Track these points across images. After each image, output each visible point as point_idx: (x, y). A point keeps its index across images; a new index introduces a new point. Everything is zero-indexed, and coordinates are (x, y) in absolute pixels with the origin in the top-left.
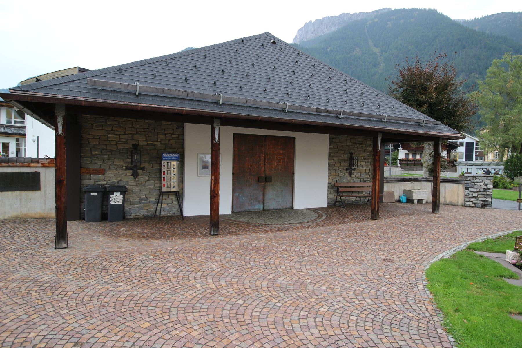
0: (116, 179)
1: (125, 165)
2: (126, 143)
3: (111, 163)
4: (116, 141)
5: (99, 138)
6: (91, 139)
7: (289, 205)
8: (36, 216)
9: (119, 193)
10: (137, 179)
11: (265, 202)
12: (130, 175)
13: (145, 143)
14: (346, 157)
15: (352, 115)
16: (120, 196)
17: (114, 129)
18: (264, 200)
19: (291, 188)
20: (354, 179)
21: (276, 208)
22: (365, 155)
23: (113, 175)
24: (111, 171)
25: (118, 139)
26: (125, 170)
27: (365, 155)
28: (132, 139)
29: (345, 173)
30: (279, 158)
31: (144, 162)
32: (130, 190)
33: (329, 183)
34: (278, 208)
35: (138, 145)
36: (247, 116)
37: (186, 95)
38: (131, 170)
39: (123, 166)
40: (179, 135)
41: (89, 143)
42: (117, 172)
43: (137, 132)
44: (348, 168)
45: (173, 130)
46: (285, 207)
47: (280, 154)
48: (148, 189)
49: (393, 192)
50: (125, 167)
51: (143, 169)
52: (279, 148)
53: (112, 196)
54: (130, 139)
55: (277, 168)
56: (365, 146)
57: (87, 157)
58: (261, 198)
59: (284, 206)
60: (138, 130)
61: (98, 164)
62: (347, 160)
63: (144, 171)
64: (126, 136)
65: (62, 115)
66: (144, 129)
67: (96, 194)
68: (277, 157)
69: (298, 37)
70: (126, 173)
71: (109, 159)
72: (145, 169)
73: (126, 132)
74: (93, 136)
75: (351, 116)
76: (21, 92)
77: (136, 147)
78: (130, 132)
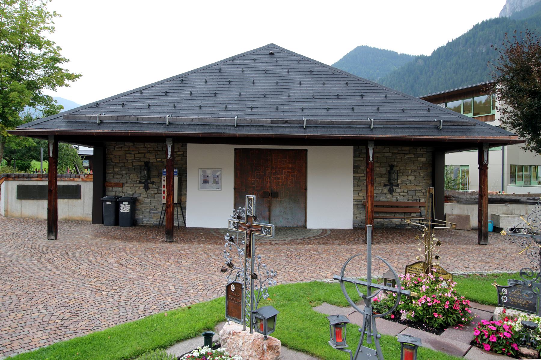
0: (131, 192)
1: (138, 180)
2: (140, 161)
3: (127, 178)
4: (132, 160)
5: (120, 158)
6: (113, 158)
7: (301, 224)
8: (78, 219)
9: (127, 203)
10: (148, 192)
11: (272, 219)
12: (142, 188)
13: (155, 160)
14: (383, 170)
15: (320, 124)
16: (128, 205)
17: (131, 149)
18: (270, 216)
19: (303, 205)
20: (397, 198)
21: (285, 225)
22: (415, 168)
23: (129, 188)
24: (127, 185)
25: (133, 158)
26: (139, 184)
27: (415, 168)
28: (145, 157)
29: (382, 190)
30: (288, 172)
31: (154, 177)
32: (143, 201)
33: (354, 201)
34: (287, 226)
35: (149, 162)
36: (187, 134)
37: (136, 119)
38: (143, 184)
39: (137, 181)
40: (183, 152)
41: (112, 161)
42: (132, 185)
43: (148, 151)
44: (387, 184)
45: (179, 147)
46: (295, 226)
47: (288, 168)
48: (157, 201)
49: (469, 216)
50: (138, 182)
51: (153, 183)
52: (288, 161)
53: (121, 205)
54: (142, 157)
55: (285, 183)
56: (413, 156)
57: (111, 173)
58: (267, 214)
59: (295, 224)
60: (149, 149)
61: (118, 179)
62: (385, 174)
63: (154, 185)
64: (139, 155)
65: (52, 142)
66: (154, 148)
67: (110, 203)
68: (285, 172)
69: (508, 8)
70: (139, 187)
71: (127, 175)
72: (155, 183)
73: (140, 151)
74: (115, 155)
75: (318, 124)
76: (22, 129)
77: (147, 164)
78: (143, 152)
